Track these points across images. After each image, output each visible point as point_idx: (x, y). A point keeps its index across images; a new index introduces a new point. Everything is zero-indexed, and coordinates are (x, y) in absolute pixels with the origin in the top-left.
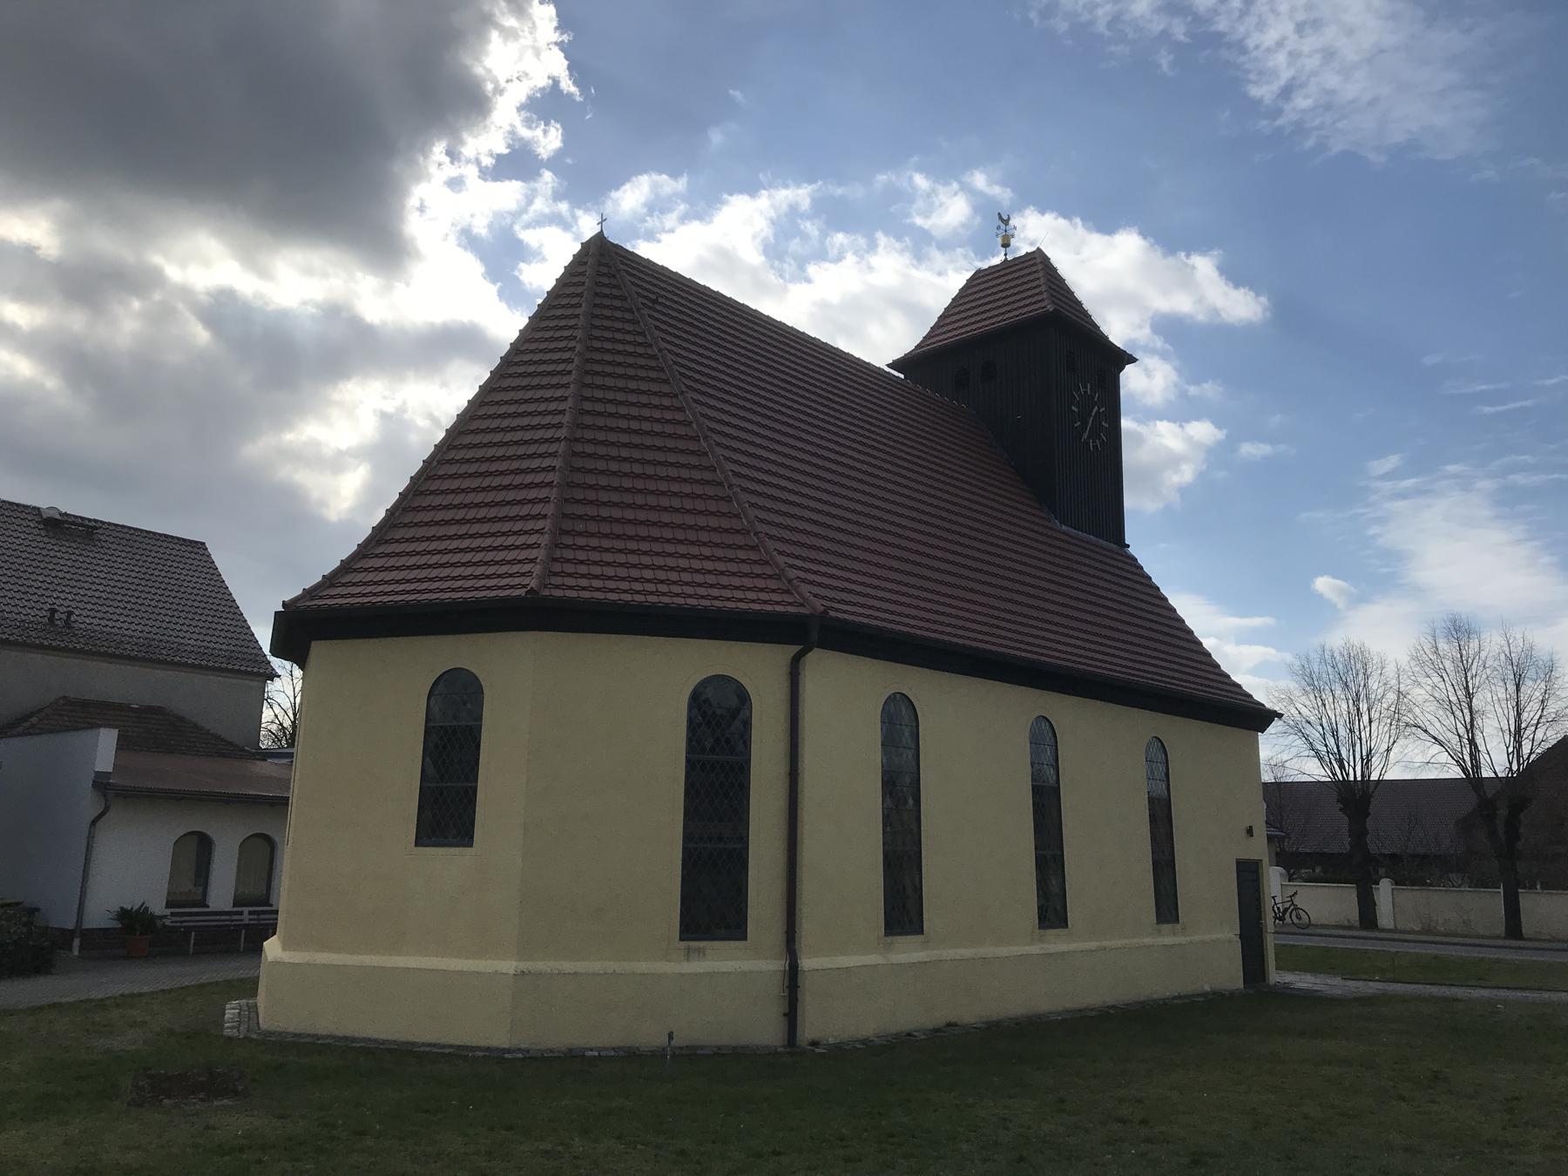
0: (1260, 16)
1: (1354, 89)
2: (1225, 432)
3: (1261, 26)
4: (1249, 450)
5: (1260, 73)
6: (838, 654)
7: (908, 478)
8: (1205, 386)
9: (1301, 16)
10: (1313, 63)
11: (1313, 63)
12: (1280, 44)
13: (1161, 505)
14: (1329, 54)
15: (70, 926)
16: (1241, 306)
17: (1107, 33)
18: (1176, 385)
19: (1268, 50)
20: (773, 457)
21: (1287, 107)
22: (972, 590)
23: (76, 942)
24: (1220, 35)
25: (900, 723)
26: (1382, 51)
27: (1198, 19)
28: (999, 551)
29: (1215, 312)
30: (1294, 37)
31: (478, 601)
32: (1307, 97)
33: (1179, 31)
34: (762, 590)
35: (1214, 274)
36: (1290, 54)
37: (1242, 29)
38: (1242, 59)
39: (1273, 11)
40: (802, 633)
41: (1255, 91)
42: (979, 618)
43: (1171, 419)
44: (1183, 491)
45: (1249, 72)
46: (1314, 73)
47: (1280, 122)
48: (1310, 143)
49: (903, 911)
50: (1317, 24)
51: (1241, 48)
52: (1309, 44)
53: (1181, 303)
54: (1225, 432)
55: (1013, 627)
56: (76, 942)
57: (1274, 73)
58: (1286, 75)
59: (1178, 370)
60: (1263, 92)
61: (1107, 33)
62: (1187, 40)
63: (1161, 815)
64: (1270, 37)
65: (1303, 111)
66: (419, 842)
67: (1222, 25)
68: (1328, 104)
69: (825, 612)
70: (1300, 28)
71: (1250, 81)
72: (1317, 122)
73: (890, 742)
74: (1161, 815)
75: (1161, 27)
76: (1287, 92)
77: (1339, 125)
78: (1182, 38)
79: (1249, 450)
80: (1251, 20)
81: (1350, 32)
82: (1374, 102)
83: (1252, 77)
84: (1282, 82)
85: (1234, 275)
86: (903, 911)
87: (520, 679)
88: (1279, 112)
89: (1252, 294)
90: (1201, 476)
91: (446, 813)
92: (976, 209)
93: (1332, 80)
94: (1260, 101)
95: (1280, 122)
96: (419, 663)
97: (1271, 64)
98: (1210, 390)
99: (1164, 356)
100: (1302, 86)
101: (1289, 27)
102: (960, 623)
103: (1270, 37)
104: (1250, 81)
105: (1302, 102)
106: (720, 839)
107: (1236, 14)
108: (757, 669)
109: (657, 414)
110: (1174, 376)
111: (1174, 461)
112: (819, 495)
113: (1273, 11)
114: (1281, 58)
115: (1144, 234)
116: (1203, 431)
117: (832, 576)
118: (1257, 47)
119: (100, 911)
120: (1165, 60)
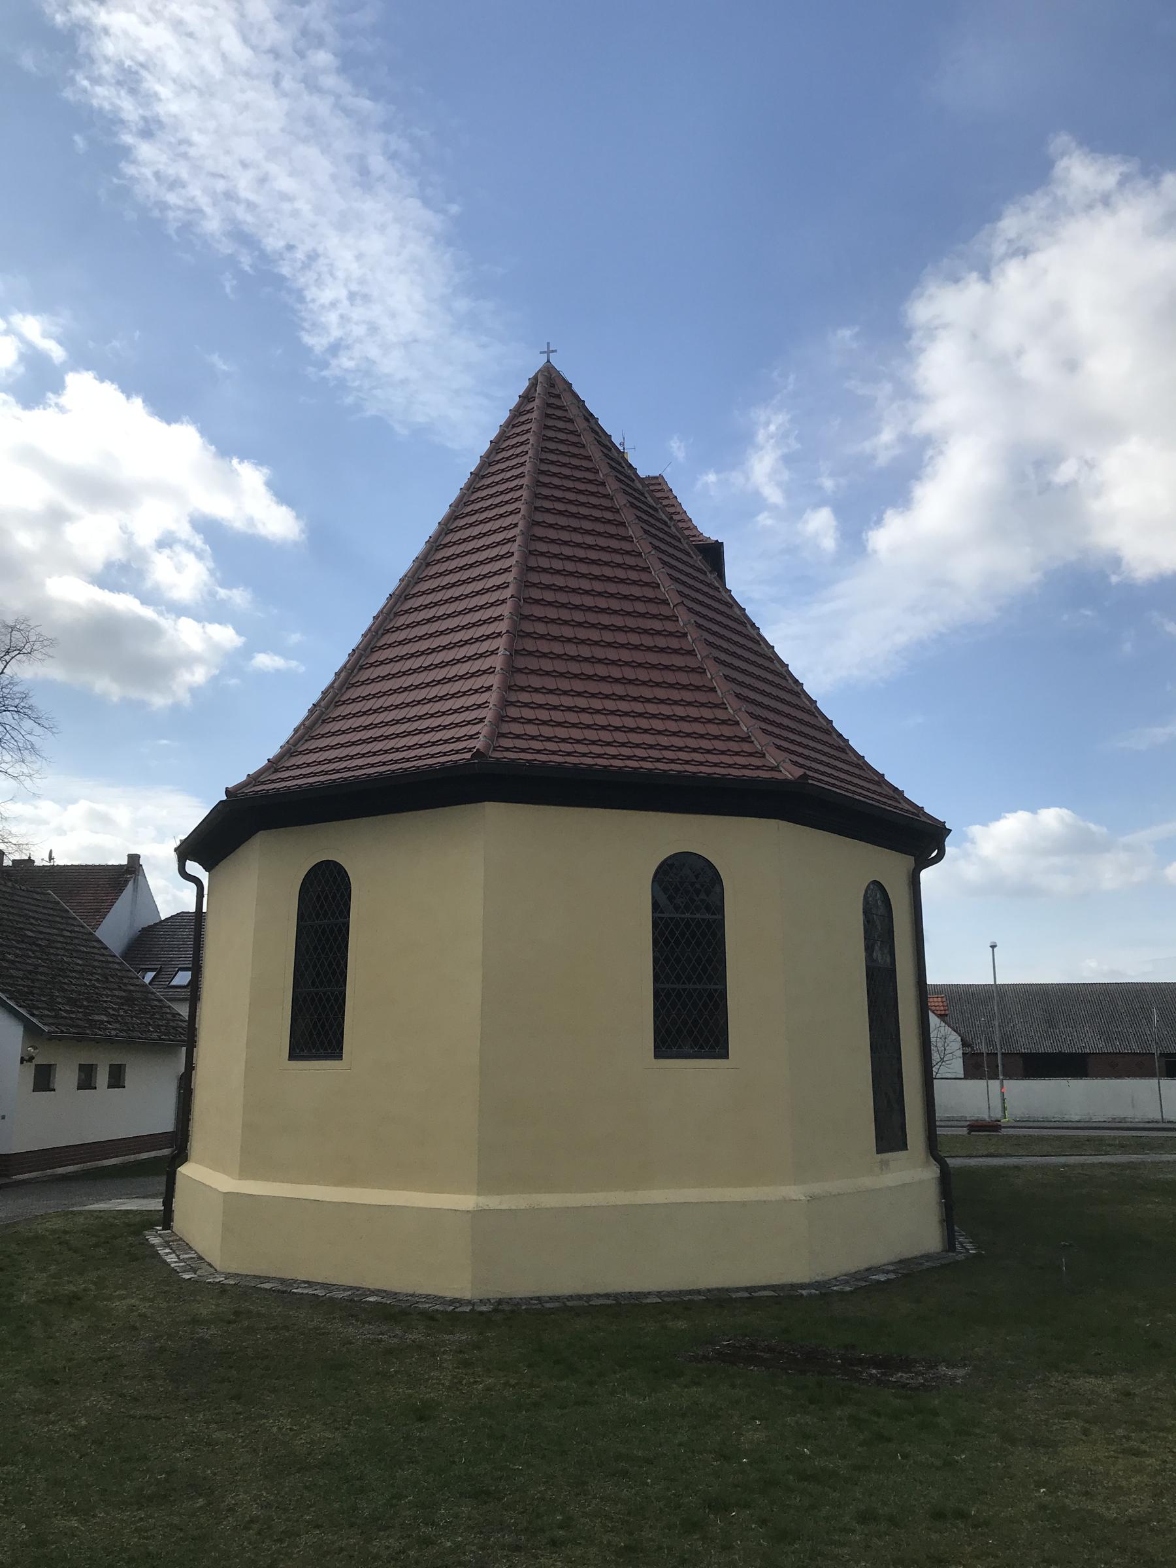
0: (319, 274)
1: (392, 364)
2: (243, 639)
3: (319, 282)
4: (265, 661)
5: (314, 324)
6: (421, 812)
8: (235, 591)
9: (354, 287)
10: (360, 331)
11: (360, 331)
12: (334, 304)
13: (170, 701)
14: (373, 329)
16: (278, 522)
17: (175, 238)
18: (205, 585)
19: (323, 306)
21: (334, 362)
24: (282, 279)
26: (416, 341)
27: (263, 256)
29: (251, 521)
30: (346, 303)
32: (351, 358)
33: (246, 261)
34: (549, 739)
35: (263, 489)
36: (342, 317)
37: (302, 280)
38: (299, 306)
39: (332, 275)
41: (308, 339)
43: (198, 619)
44: (194, 691)
45: (304, 320)
46: (359, 340)
47: (324, 373)
48: (349, 400)
50: (366, 298)
51: (301, 299)
52: (358, 313)
53: (220, 507)
54: (243, 639)
57: (322, 328)
58: (336, 333)
59: (212, 572)
60: (316, 342)
61: (175, 238)
62: (251, 271)
64: (327, 295)
65: (346, 370)
67: (285, 270)
68: (367, 370)
69: (805, 776)
70: (352, 296)
71: (303, 329)
72: (357, 383)
75: (229, 251)
76: (335, 348)
77: (374, 392)
78: (247, 268)
79: (265, 661)
80: (311, 275)
81: (393, 315)
82: (404, 382)
83: (306, 325)
84: (332, 340)
85: (281, 492)
88: (326, 365)
89: (294, 514)
90: (214, 681)
92: (23, 358)
93: (374, 352)
94: (310, 349)
95: (324, 373)
97: (323, 319)
98: (239, 597)
99: (200, 556)
100: (348, 347)
101: (343, 294)
103: (327, 295)
104: (303, 329)
105: (345, 362)
107: (299, 265)
109: (581, 553)
110: (205, 576)
111: (189, 660)
113: (332, 275)
114: (333, 317)
115: (203, 432)
116: (225, 635)
117: (792, 741)
118: (313, 301)
120: (229, 284)
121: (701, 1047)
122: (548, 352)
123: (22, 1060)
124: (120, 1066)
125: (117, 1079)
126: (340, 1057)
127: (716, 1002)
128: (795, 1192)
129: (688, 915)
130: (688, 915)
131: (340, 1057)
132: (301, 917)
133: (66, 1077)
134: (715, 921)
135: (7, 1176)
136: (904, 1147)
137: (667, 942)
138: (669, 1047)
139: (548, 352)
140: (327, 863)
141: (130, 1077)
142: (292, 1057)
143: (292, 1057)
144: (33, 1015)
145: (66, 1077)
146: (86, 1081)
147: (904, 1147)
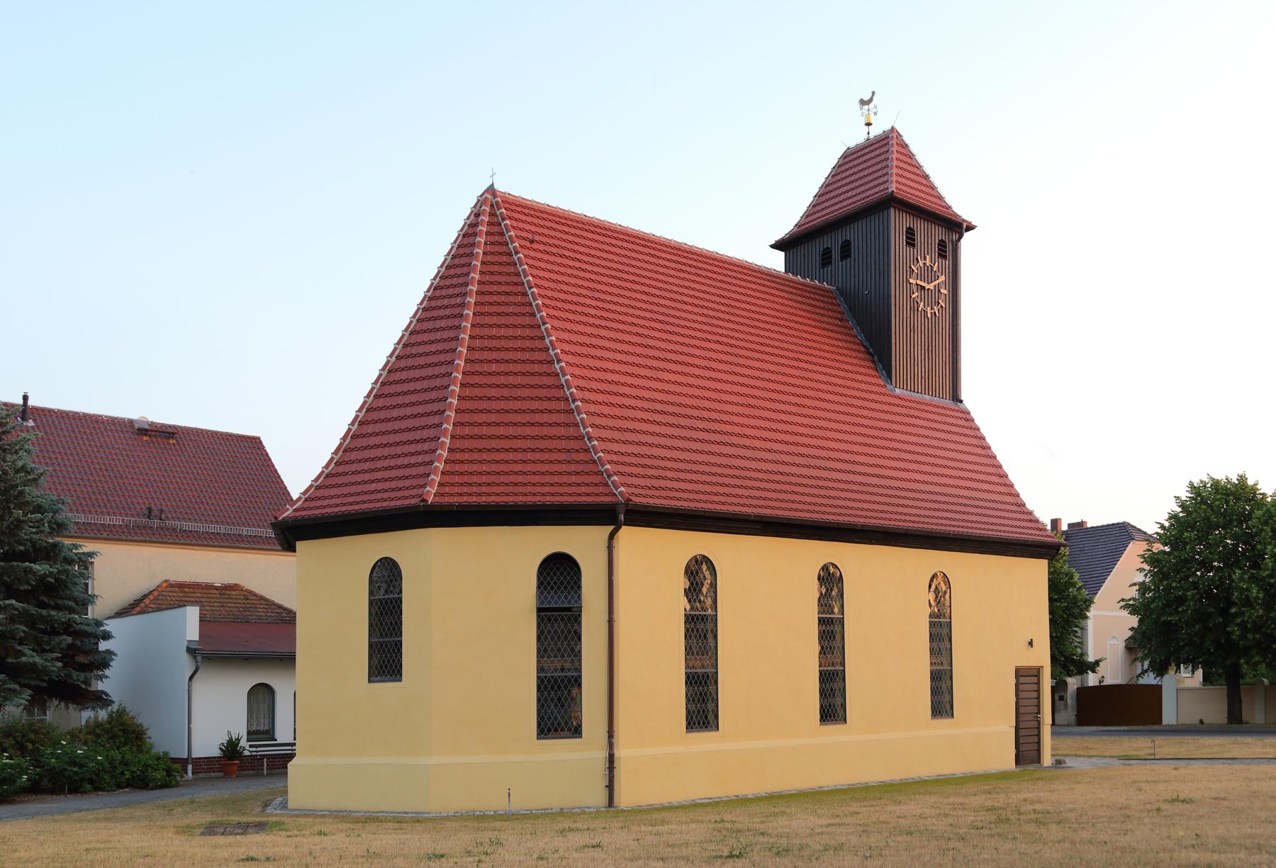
7: (971, 479)
15: (185, 756)
20: (682, 331)
22: (783, 463)
23: (190, 767)
25: (699, 575)
28: (634, 263)
31: (357, 513)
40: (608, 515)
42: (713, 290)
49: (702, 709)
55: (703, 288)
56: (190, 767)
63: (940, 634)
66: (370, 681)
73: (693, 592)
74: (940, 634)
86: (702, 709)
87: (426, 556)
91: (386, 660)
96: (365, 551)
102: (726, 317)
106: (562, 670)
108: (582, 542)
112: (410, 423)
119: (207, 745)
136: (576, 732)
147: (576, 732)
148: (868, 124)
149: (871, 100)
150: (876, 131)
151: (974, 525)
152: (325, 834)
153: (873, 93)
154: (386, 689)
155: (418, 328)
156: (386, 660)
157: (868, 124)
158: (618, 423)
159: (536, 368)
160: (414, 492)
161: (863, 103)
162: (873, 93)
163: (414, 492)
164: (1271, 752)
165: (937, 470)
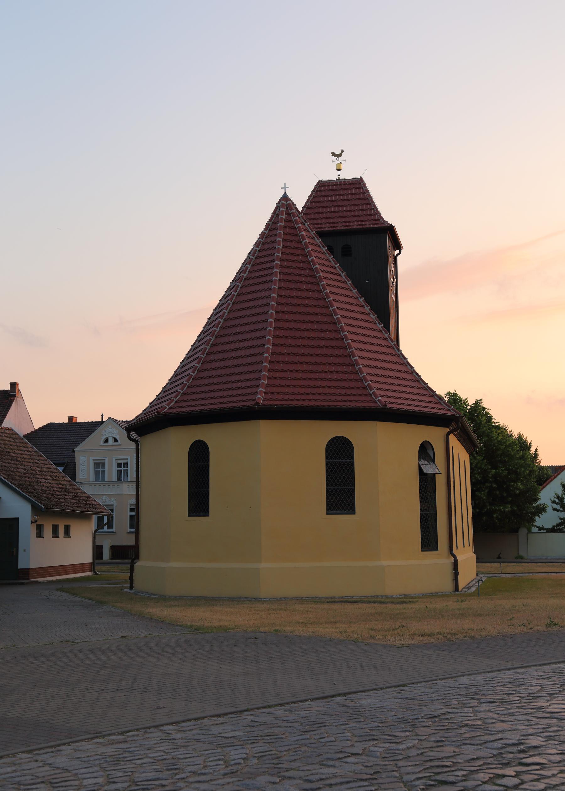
91: (199, 503)
121: (345, 510)
122: (285, 188)
123: (32, 522)
124: (67, 525)
125: (67, 534)
126: (208, 515)
127: (351, 494)
128: (385, 563)
129: (340, 461)
130: (340, 461)
131: (208, 515)
132: (190, 461)
133: (48, 531)
134: (350, 462)
135: (28, 579)
136: (436, 549)
137: (331, 471)
138: (332, 510)
139: (285, 188)
140: (199, 441)
141: (72, 532)
142: (328, 513)
143: (328, 513)
144: (30, 496)
145: (48, 531)
146: (55, 534)
147: (436, 549)
148: (339, 170)
149: (340, 155)
150: (347, 174)
151: (198, 403)
152: (122, 637)
153: (342, 151)
154: (342, 520)
155: (237, 300)
156: (199, 503)
157: (339, 170)
158: (313, 360)
159: (328, 335)
160: (249, 397)
161: (333, 154)
162: (342, 151)
163: (249, 397)
164: (1, 777)
165: (395, 388)
